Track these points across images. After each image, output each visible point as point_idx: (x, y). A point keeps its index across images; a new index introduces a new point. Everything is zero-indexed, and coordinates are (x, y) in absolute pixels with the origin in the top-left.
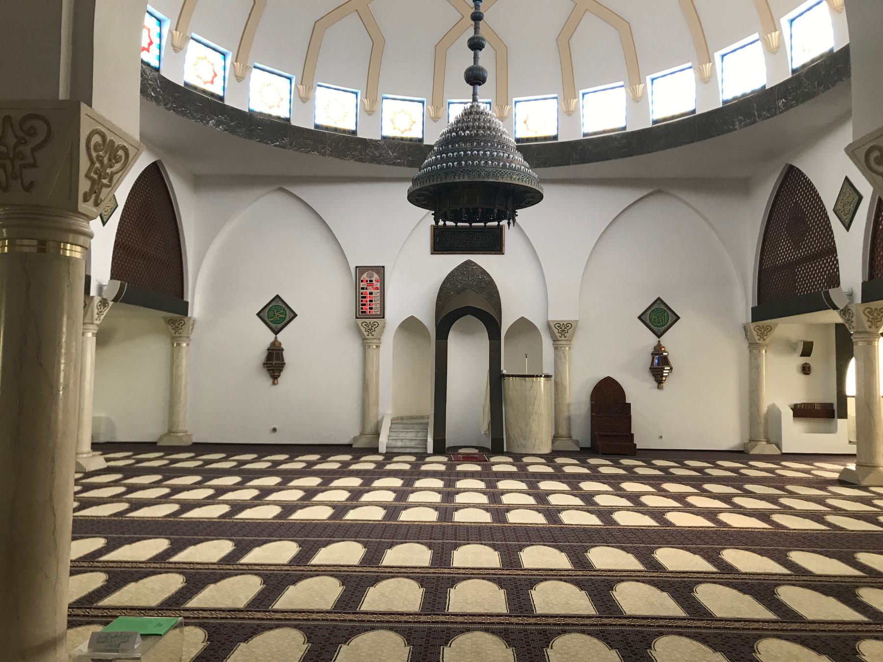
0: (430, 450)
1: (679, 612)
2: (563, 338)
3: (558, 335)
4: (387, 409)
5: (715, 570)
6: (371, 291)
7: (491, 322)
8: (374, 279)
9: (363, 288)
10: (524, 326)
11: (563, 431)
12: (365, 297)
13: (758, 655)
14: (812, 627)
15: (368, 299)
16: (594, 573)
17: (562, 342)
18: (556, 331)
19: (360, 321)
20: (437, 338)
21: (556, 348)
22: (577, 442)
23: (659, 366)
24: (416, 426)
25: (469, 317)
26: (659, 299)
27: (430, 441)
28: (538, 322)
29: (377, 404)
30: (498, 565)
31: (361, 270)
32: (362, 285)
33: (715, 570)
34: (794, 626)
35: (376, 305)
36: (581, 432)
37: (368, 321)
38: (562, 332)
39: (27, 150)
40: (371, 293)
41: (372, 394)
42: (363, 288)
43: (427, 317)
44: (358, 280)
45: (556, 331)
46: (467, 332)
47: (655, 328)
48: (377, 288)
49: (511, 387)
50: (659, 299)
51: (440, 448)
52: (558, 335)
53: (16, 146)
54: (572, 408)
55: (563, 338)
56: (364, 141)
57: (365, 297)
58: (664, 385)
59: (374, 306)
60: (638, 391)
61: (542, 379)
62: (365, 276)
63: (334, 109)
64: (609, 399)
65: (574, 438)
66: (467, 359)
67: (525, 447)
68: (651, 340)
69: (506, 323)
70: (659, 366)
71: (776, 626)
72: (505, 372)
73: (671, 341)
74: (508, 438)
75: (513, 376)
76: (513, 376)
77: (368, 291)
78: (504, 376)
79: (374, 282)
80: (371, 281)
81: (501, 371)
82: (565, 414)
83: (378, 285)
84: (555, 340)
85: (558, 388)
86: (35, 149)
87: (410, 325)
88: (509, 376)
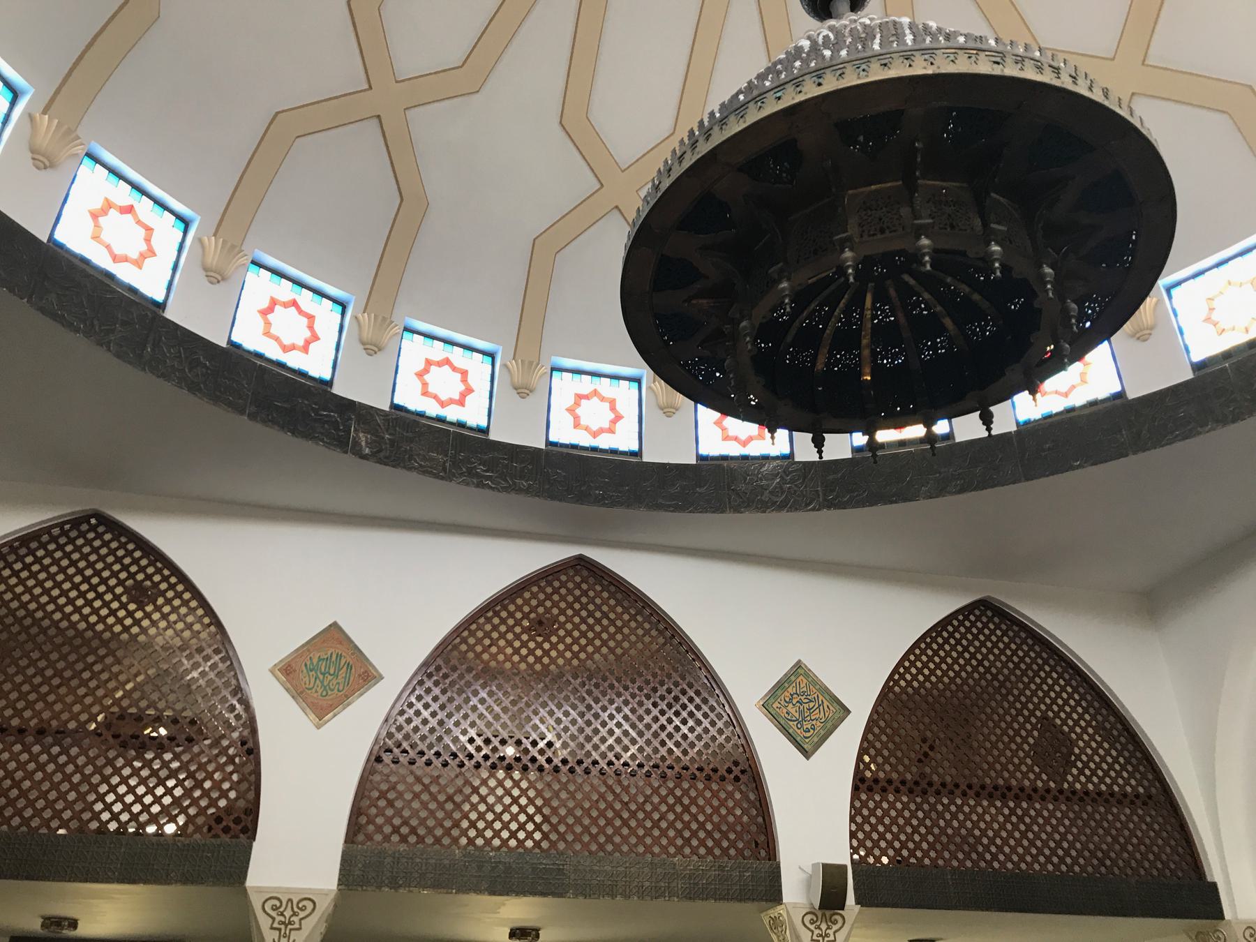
56: (348, 406)
63: (282, 321)
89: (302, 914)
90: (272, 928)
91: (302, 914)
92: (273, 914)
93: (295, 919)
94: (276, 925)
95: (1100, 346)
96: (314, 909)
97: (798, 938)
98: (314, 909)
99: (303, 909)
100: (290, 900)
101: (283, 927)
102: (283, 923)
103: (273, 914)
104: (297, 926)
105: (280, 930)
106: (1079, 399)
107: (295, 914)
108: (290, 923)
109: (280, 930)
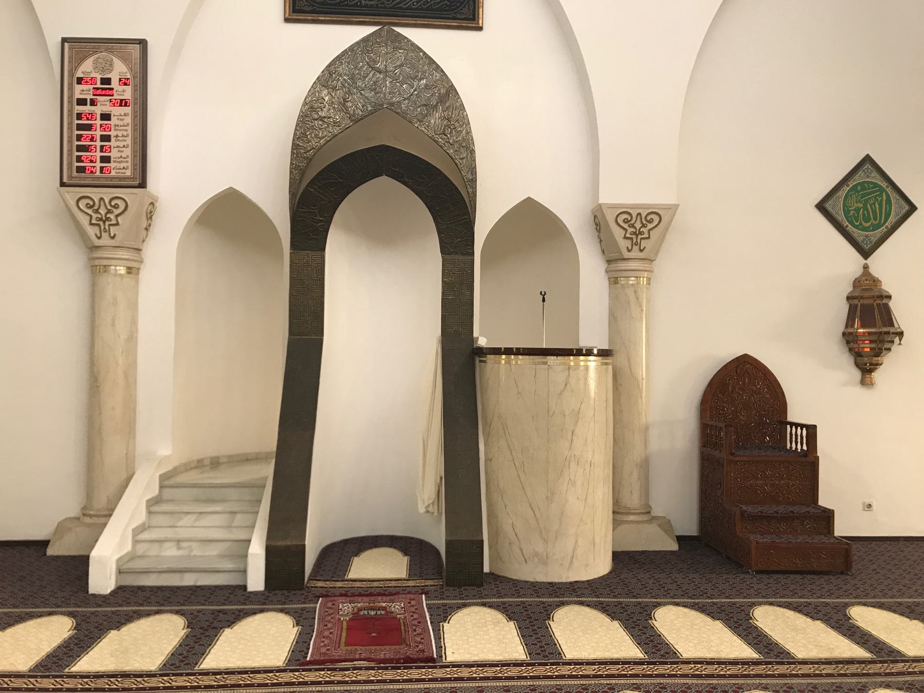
0: (256, 581)
1: (636, 653)
2: (635, 253)
3: (624, 244)
4: (160, 443)
5: (754, 655)
6: (107, 109)
7: (448, 200)
8: (114, 77)
9: (82, 102)
10: (533, 223)
11: (633, 500)
12: (89, 127)
13: (551, 623)
14: (805, 669)
15: (98, 133)
16: (565, 670)
17: (632, 265)
18: (618, 233)
19: (71, 195)
20: (294, 245)
21: (614, 281)
22: (666, 525)
23: (869, 327)
24: (233, 493)
25: (384, 182)
26: (868, 159)
27: (257, 551)
28: (570, 211)
29: (130, 429)
30: (403, 574)
31: (77, 48)
32: (80, 91)
33: (754, 655)
34: (782, 669)
35: (122, 153)
36: (675, 501)
37: (95, 194)
38: (630, 235)
39: (112, 216)
40: (106, 117)
41: (112, 401)
42: (82, 102)
43: (273, 199)
44: (69, 77)
45: (618, 233)
46: (381, 235)
47: (892, 219)
48: (123, 103)
49: (502, 382)
50: (868, 159)
51: (287, 580)
52: (624, 244)
53: (106, 214)
54: (654, 434)
55: (635, 253)
57: (89, 127)
58: (877, 375)
59: (114, 154)
60: (817, 389)
61: (593, 362)
62: (87, 68)
64: (743, 412)
65: (657, 511)
66: (380, 312)
67: (544, 561)
68: (844, 262)
69: (488, 215)
70: (869, 327)
71: (760, 669)
72: (482, 342)
73: (893, 264)
74: (495, 533)
75: (509, 351)
76: (509, 351)
77: (98, 110)
78: (482, 352)
79: (115, 84)
80: (106, 81)
81: (472, 340)
82: (636, 454)
83: (127, 93)
84: (612, 259)
85: (622, 387)
86: (117, 216)
87: (226, 215)
88: (497, 351)
89: (650, 226)
90: (625, 238)
91: (650, 226)
92: (90, 211)
93: (112, 216)
94: (628, 235)
95: (56, 554)
96: (660, 222)
97: (921, 673)
98: (660, 222)
99: (651, 221)
100: (102, 199)
101: (634, 236)
102: (101, 219)
103: (626, 226)
104: (646, 235)
105: (632, 239)
106: (311, 567)
107: (644, 226)
108: (641, 233)
109: (632, 239)
